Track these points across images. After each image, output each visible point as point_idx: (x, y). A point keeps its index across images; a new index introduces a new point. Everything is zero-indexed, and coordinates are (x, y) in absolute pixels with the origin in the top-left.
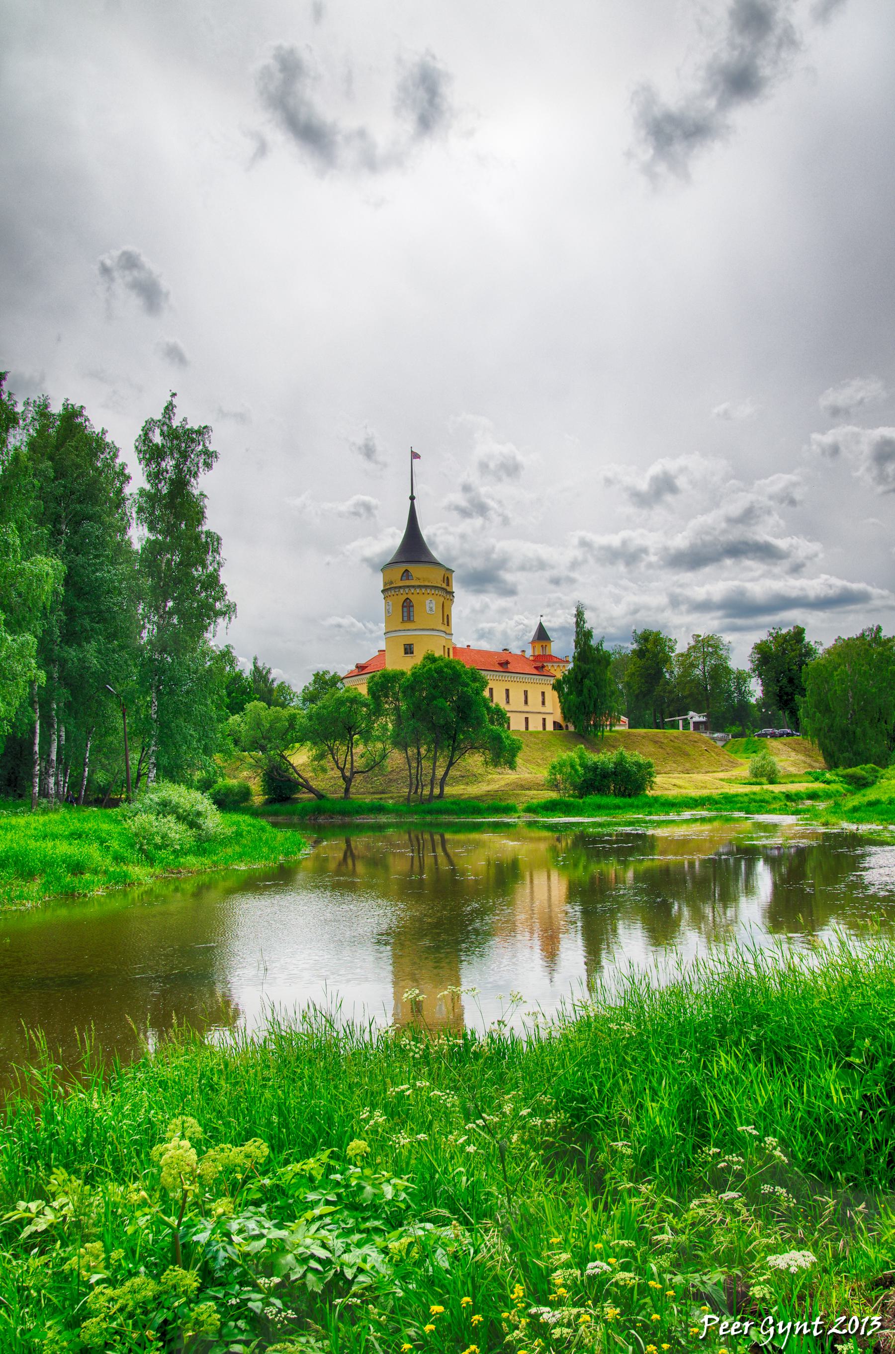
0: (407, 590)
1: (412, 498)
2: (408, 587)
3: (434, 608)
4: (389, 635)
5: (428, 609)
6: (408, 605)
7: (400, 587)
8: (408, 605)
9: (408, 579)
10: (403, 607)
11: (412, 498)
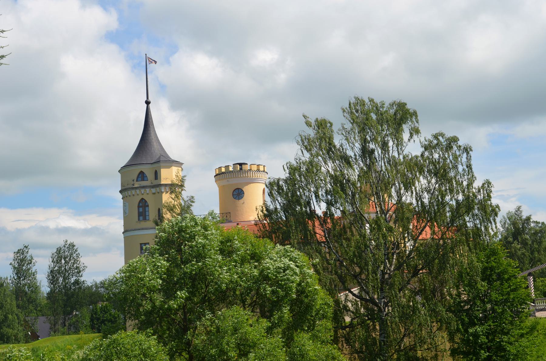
0: (143, 191)
1: (148, 103)
8: (143, 204)
10: (139, 207)
11: (148, 103)
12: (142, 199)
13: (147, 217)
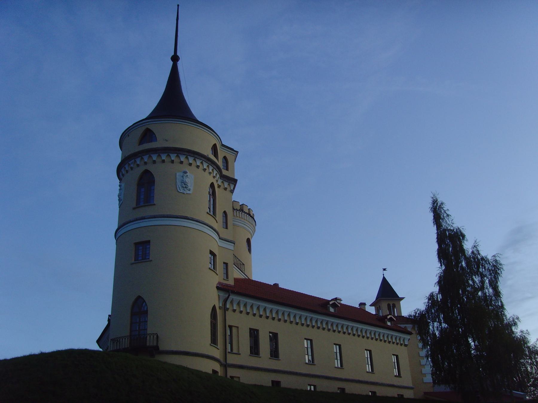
1: (175, 59)
11: (175, 59)
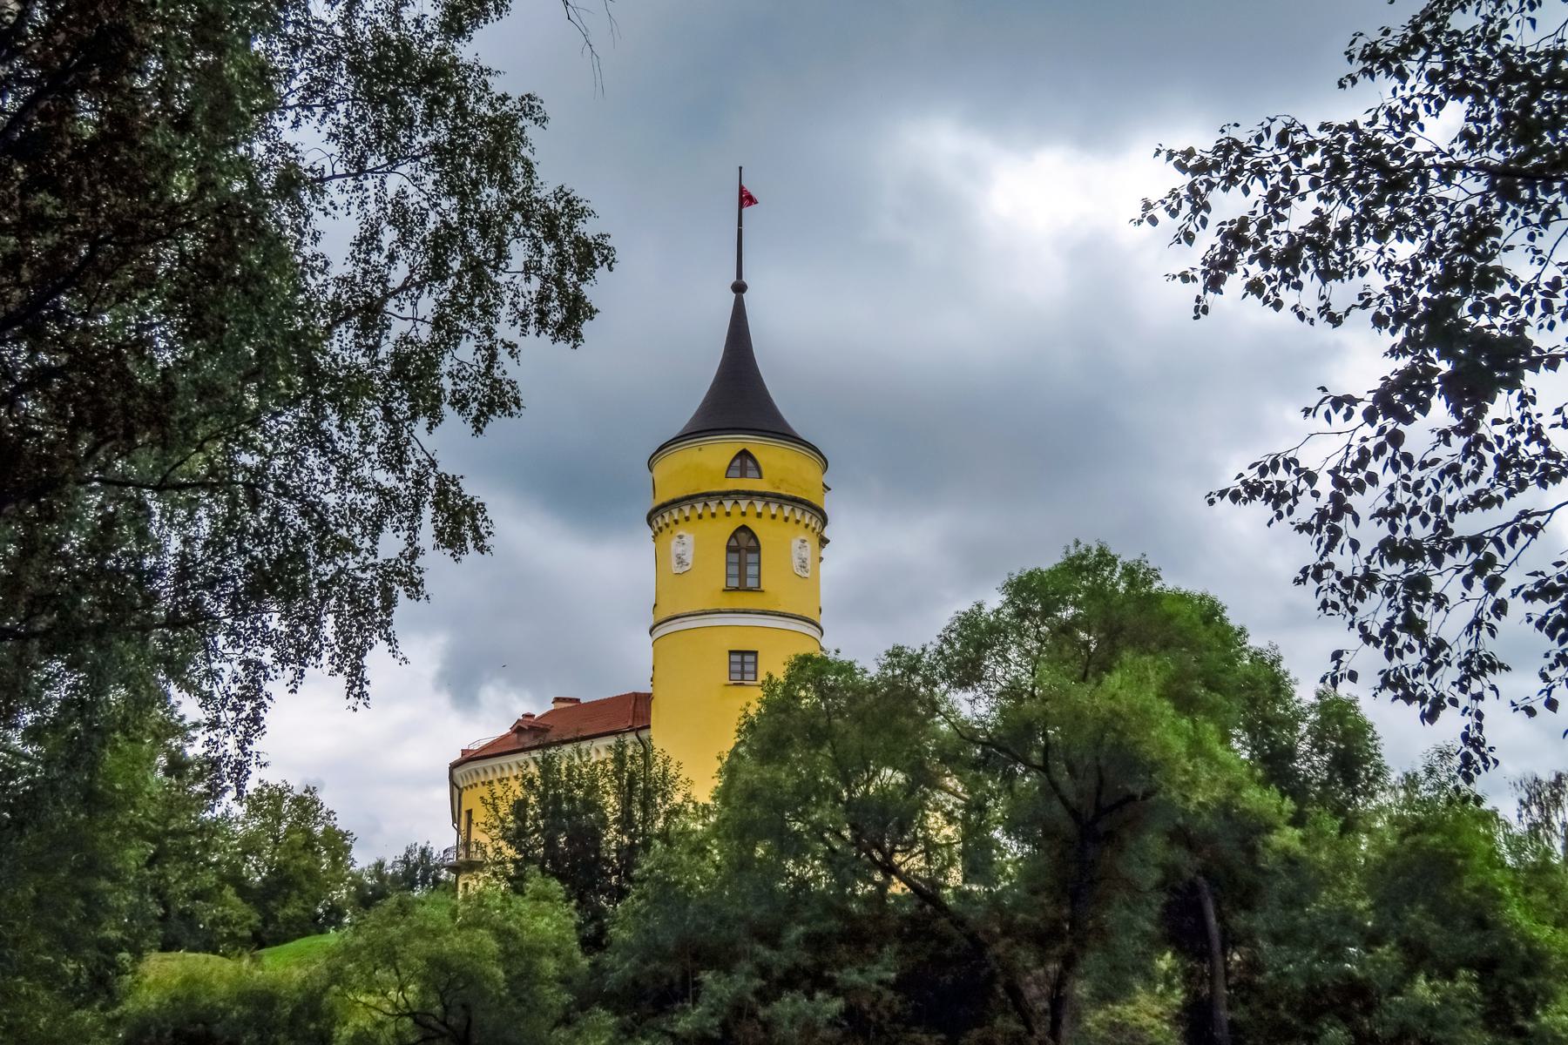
0: (744, 505)
1: (739, 288)
2: (749, 495)
3: (688, 558)
4: (659, 632)
5: (796, 562)
6: (743, 545)
7: (726, 494)
8: (743, 545)
9: (743, 475)
11: (739, 288)
12: (744, 528)
13: (751, 583)
